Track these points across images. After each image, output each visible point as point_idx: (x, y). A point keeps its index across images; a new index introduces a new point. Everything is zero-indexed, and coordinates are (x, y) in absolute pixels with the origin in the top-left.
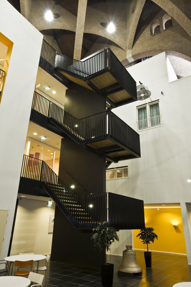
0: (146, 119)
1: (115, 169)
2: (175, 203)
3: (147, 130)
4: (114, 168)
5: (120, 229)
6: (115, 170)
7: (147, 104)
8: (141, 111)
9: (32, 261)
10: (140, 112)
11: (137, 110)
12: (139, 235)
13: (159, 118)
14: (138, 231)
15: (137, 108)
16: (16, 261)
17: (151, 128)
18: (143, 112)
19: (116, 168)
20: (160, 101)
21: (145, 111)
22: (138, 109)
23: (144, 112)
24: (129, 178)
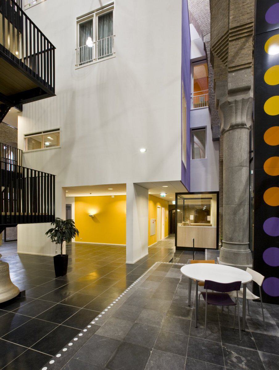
0: (84, 46)
1: (43, 134)
2: (168, 182)
3: (91, 65)
4: (41, 133)
5: (20, 223)
6: (42, 136)
7: (94, 14)
8: (107, 18)
9: (240, 282)
10: (83, 31)
11: (79, 25)
12: (51, 231)
13: (111, 40)
14: (49, 226)
15: (78, 22)
16: (206, 281)
17: (98, 61)
18: (101, 24)
19: (44, 132)
20: (114, 5)
21: (91, 29)
22: (80, 25)
23: (89, 32)
24: (60, 148)
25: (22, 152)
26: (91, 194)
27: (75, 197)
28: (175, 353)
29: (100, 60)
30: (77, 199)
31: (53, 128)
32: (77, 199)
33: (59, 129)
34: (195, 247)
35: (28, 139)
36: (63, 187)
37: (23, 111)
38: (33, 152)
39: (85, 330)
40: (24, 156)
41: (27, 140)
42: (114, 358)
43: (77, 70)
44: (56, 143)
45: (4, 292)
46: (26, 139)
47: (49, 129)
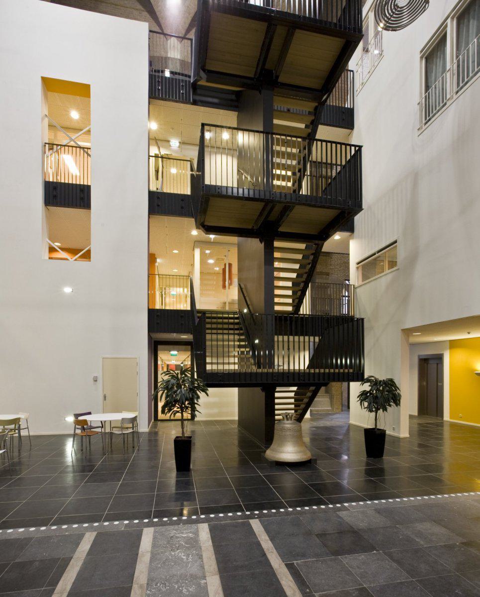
19: (379, 252)
24: (398, 269)
25: (354, 287)
26: (469, 333)
27: (451, 341)
28: (407, 571)
29: (427, 125)
30: (453, 345)
31: (388, 243)
32: (453, 345)
33: (395, 242)
34: (378, 427)
35: (362, 267)
36: (402, 330)
37: (355, 232)
38: (371, 281)
39: (331, 506)
40: (356, 293)
41: (360, 269)
42: (331, 534)
43: (420, 136)
44: (393, 264)
45: (293, 453)
46: (359, 268)
47: (384, 245)
